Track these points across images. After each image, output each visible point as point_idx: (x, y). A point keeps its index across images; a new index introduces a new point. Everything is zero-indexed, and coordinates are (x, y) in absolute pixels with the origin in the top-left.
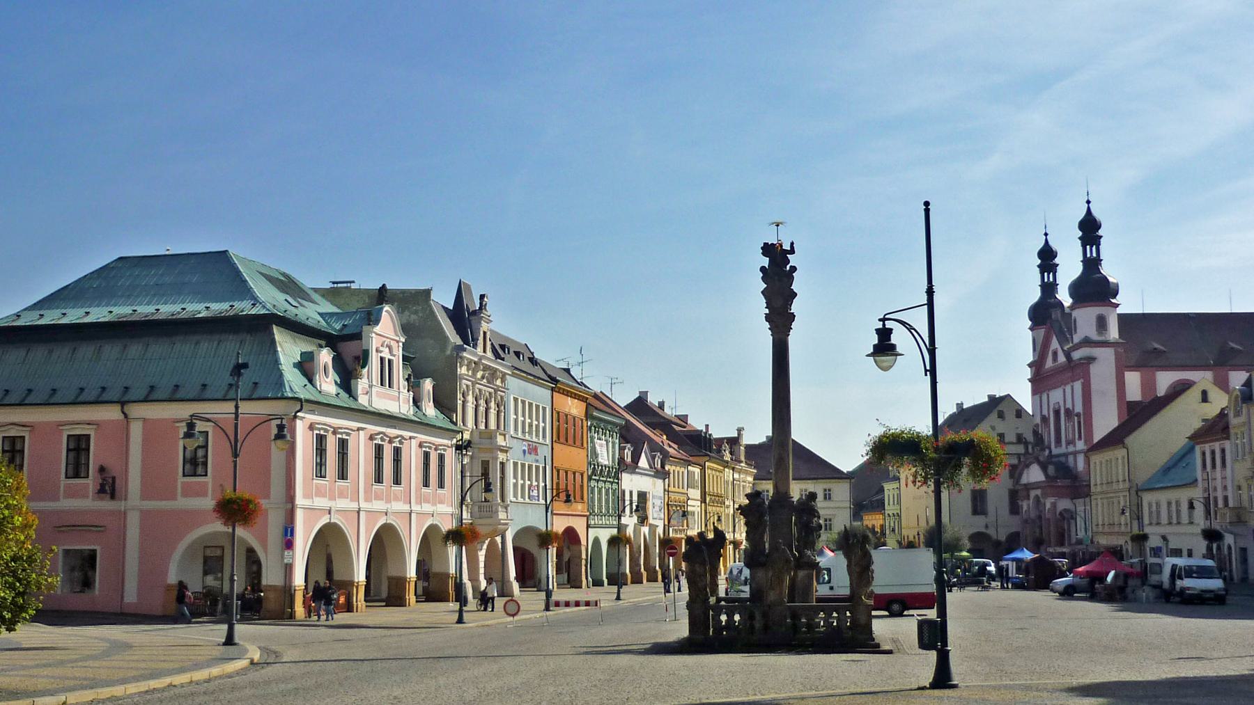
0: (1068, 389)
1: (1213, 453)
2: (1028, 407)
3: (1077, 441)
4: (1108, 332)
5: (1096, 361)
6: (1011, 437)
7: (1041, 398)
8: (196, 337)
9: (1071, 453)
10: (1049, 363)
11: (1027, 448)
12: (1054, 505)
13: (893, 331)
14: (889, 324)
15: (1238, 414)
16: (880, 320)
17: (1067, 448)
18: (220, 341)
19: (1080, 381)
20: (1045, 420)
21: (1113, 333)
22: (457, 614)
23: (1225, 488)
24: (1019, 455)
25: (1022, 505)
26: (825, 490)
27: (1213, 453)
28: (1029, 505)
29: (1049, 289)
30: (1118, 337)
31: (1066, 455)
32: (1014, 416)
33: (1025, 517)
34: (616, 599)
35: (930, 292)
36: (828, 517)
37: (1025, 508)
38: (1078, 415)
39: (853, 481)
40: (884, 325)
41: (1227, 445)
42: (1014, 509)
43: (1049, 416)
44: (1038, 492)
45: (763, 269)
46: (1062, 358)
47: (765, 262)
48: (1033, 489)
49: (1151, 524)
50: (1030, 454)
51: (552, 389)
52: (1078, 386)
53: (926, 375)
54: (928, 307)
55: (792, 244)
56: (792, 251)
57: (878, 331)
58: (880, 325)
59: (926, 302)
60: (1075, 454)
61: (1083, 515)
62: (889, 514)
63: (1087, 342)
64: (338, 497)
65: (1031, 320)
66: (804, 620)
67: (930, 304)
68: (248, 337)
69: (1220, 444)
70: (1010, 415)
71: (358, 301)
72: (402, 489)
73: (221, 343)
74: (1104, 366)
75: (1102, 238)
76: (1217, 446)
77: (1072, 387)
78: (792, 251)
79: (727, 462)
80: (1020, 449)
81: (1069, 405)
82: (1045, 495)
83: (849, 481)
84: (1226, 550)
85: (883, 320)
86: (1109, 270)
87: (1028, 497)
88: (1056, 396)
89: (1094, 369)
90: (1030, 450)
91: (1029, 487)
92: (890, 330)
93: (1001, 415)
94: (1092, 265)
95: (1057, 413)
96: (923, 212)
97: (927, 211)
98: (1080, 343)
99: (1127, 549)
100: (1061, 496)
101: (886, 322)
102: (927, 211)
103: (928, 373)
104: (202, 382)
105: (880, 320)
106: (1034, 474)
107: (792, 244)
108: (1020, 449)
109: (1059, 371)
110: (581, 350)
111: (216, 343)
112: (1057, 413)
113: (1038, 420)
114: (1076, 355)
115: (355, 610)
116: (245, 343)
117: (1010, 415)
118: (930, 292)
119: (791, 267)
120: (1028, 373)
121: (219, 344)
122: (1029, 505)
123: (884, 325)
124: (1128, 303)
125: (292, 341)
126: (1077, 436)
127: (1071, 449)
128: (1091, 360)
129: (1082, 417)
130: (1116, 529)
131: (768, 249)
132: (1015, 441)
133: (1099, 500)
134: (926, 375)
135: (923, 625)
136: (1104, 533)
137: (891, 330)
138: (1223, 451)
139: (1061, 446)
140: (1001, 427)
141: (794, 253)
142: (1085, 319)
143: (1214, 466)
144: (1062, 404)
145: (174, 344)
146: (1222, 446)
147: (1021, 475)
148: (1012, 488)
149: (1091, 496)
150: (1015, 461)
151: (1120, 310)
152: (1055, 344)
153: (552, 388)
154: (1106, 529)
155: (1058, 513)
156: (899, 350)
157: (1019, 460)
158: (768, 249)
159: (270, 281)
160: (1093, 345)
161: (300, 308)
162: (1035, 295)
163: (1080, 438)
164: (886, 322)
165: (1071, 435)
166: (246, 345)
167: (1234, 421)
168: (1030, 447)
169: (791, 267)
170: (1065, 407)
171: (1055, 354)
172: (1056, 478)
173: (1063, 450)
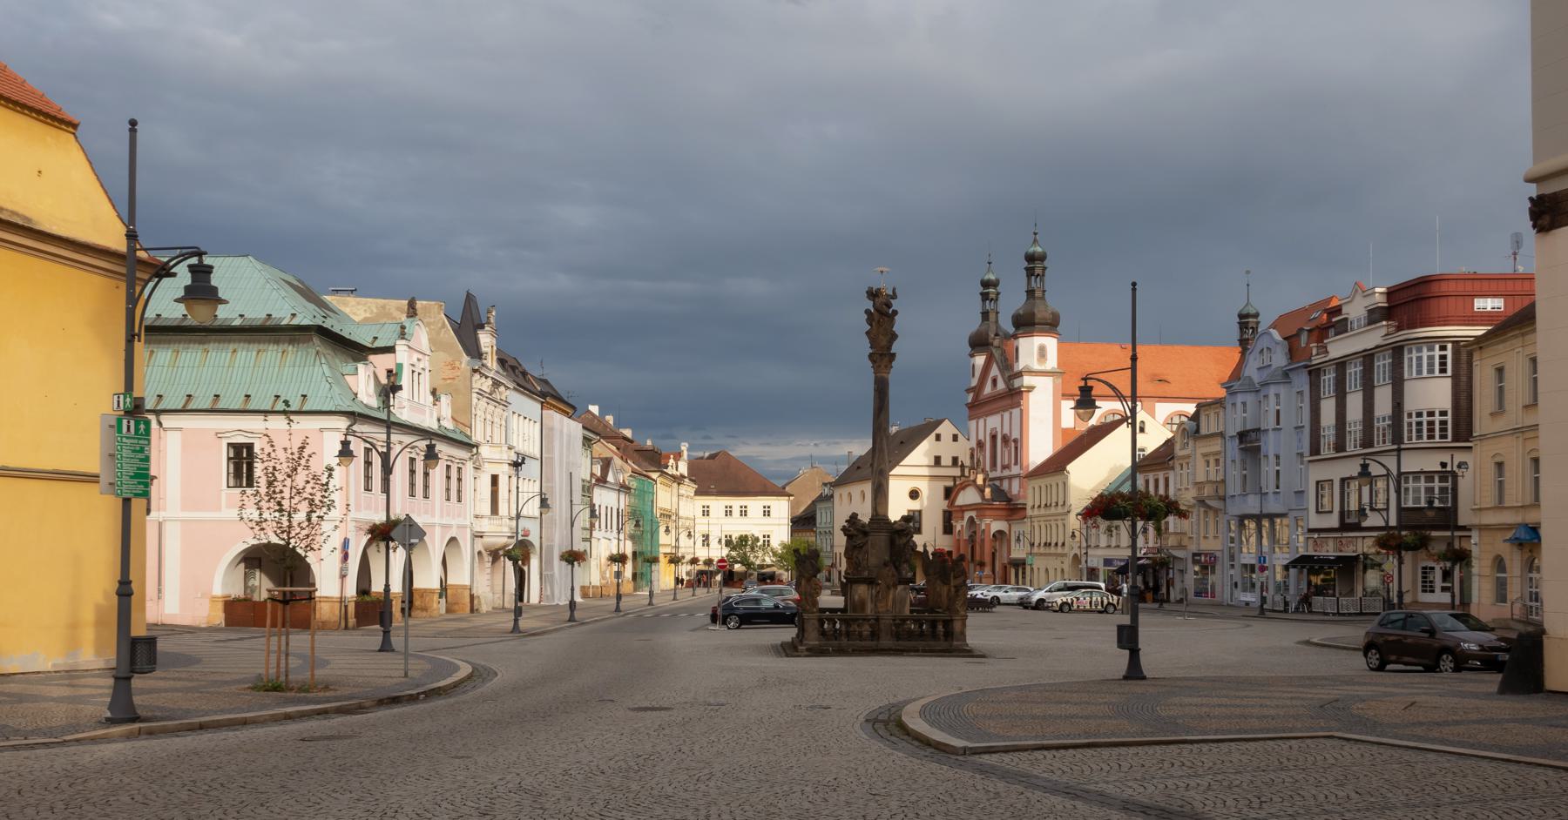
0: (1006, 415)
1: (1157, 481)
3: (1013, 466)
9: (1005, 478)
10: (988, 389)
13: (214, 270)
14: (1090, 383)
15: (1183, 448)
16: (1083, 379)
17: (1002, 472)
22: (513, 623)
24: (954, 478)
27: (1157, 481)
28: (962, 526)
30: (1056, 366)
31: (1001, 479)
33: (957, 538)
35: (1134, 359)
36: (766, 534)
39: (792, 498)
40: (1086, 383)
41: (1171, 475)
42: (948, 529)
44: (973, 514)
47: (869, 305)
48: (967, 510)
50: (966, 477)
51: (542, 403)
55: (894, 290)
56: (894, 296)
58: (1082, 384)
60: (1010, 478)
66: (913, 626)
67: (1134, 369)
68: (290, 348)
71: (365, 311)
72: (372, 496)
73: (260, 353)
76: (1161, 476)
78: (894, 296)
80: (956, 472)
81: (1006, 431)
82: (981, 517)
83: (787, 498)
85: (1085, 379)
87: (962, 518)
90: (967, 474)
91: (963, 509)
95: (994, 437)
97: (1134, 290)
101: (1088, 381)
102: (1134, 290)
105: (1083, 379)
107: (894, 290)
108: (956, 472)
109: (996, 398)
110: (542, 362)
111: (254, 353)
112: (994, 437)
115: (268, 622)
116: (288, 353)
118: (1134, 359)
119: (893, 311)
121: (258, 353)
122: (962, 526)
123: (1086, 383)
125: (332, 353)
126: (1013, 462)
127: (1006, 473)
130: (1053, 550)
131: (873, 294)
132: (950, 464)
137: (211, 267)
138: (1167, 480)
139: (996, 470)
141: (896, 298)
144: (999, 430)
146: (1166, 476)
150: (950, 484)
152: (994, 371)
154: (1042, 550)
160: (1034, 374)
164: (1088, 381)
165: (1006, 460)
167: (1179, 452)
168: (967, 471)
169: (893, 311)
170: (1002, 431)
171: (995, 381)
172: (993, 500)
173: (998, 473)
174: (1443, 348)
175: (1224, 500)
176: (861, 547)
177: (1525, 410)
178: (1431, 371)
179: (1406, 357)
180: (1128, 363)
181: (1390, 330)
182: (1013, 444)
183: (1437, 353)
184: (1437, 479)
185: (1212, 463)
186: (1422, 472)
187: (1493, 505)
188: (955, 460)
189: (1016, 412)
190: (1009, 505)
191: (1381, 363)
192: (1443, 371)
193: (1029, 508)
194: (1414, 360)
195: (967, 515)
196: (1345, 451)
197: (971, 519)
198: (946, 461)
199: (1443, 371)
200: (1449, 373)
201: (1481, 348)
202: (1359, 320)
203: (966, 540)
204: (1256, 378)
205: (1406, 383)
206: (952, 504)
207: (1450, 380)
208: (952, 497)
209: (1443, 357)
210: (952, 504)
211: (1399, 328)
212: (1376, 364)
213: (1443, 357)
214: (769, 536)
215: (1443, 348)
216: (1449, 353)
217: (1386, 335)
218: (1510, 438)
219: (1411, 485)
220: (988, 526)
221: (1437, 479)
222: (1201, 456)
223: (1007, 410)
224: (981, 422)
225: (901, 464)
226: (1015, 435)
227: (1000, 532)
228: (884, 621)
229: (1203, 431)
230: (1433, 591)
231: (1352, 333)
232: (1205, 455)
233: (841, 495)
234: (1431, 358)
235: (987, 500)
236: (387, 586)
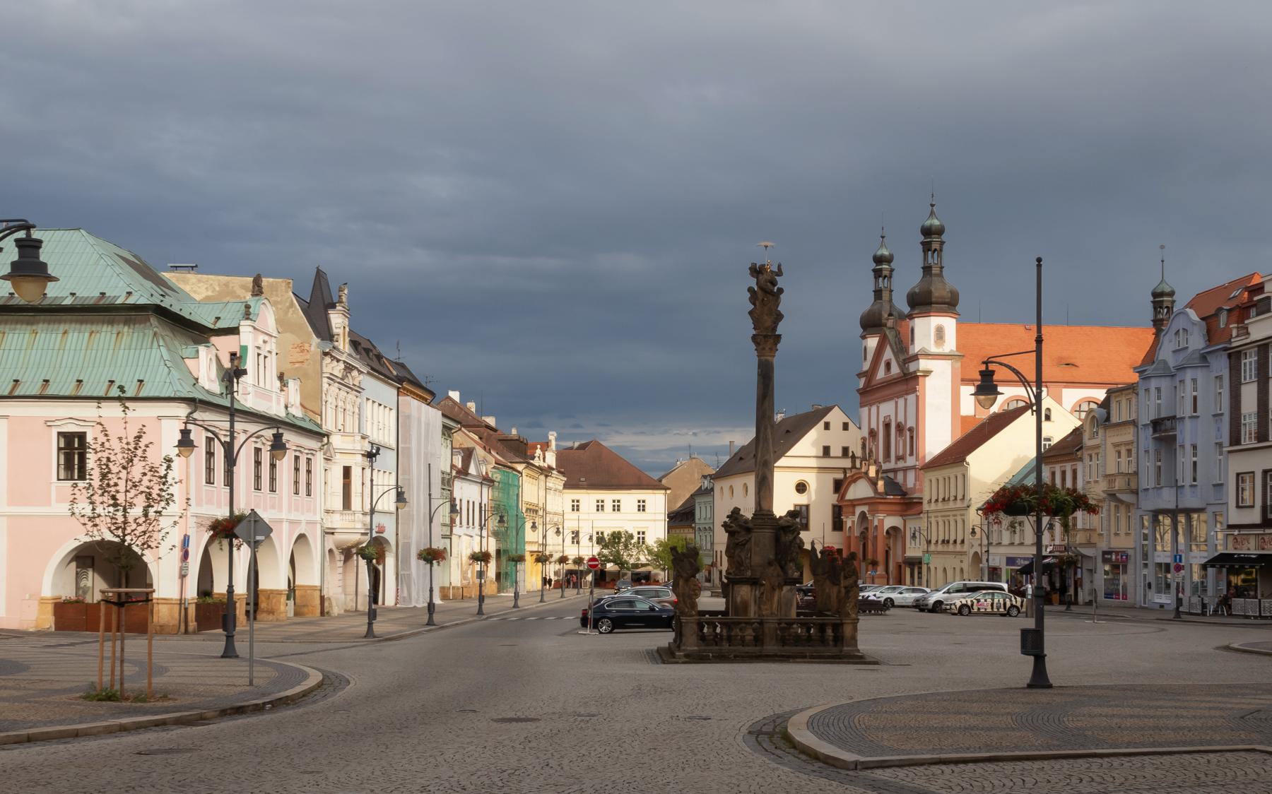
0: (901, 402)
1: (1064, 473)
5: (932, 374)
6: (836, 451)
7: (870, 410)
8: (62, 327)
10: (881, 374)
11: (854, 462)
13: (43, 245)
14: (991, 367)
16: (984, 363)
17: (896, 463)
18: (91, 333)
20: (873, 433)
24: (845, 470)
25: (846, 522)
26: (614, 501)
27: (1064, 473)
31: (895, 471)
34: (478, 614)
35: (1039, 341)
36: (641, 530)
37: (849, 524)
39: (668, 492)
40: (987, 367)
42: (838, 525)
44: (865, 509)
45: (750, 290)
46: (895, 370)
47: (753, 282)
53: (1033, 415)
54: (1037, 354)
57: (981, 373)
58: (983, 368)
59: (1035, 349)
60: (905, 470)
61: (925, 534)
62: (699, 528)
66: (799, 631)
68: (126, 329)
69: (1071, 465)
75: (945, 244)
76: (1068, 467)
78: (780, 273)
79: (1084, 504)
80: (847, 463)
81: (901, 419)
85: (986, 363)
87: (853, 513)
90: (858, 465)
91: (854, 503)
92: (993, 372)
95: (887, 426)
96: (1036, 268)
100: (890, 514)
103: (1035, 413)
104: (43, 378)
105: (984, 363)
108: (847, 463)
109: (889, 384)
111: (87, 335)
112: (887, 426)
118: (1039, 341)
122: (853, 522)
123: (987, 367)
126: (908, 452)
127: (901, 464)
131: (756, 271)
132: (841, 455)
134: (1033, 415)
135: (1025, 633)
136: (939, 553)
138: (1075, 472)
139: (890, 462)
144: (893, 418)
145: (37, 333)
150: (840, 476)
152: (888, 354)
153: (398, 388)
154: (940, 548)
155: (885, 531)
156: (51, 271)
157: (845, 475)
158: (756, 271)
159: (130, 265)
161: (167, 297)
166: (125, 338)
167: (1088, 442)
169: (778, 288)
171: (888, 365)
173: (892, 465)
175: (1137, 494)
180: (1033, 346)
182: (908, 433)
189: (911, 398)
195: (858, 510)
197: (863, 515)
204: (1172, 362)
210: (842, 498)
214: (643, 533)
220: (882, 521)
222: (1111, 446)
224: (874, 409)
225: (787, 454)
226: (911, 423)
227: (895, 529)
229: (1114, 419)
232: (1115, 445)
235: (880, 494)
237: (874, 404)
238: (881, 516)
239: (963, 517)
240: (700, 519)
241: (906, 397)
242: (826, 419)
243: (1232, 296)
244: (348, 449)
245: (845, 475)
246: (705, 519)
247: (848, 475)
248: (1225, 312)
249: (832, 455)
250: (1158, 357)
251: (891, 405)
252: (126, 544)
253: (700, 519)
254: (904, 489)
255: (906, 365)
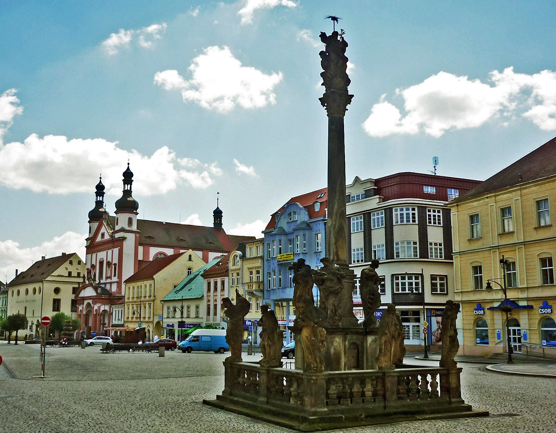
0: (110, 252)
1: (216, 283)
2: (84, 260)
4: (536, 106)
6: (74, 274)
9: (108, 283)
10: (99, 239)
12: (99, 308)
17: (106, 280)
19: (118, 248)
20: (93, 267)
21: (134, 227)
23: (216, 300)
24: (79, 283)
27: (216, 283)
29: (99, 204)
31: (105, 284)
32: (77, 264)
33: (79, 313)
38: (115, 264)
41: (226, 279)
43: (96, 264)
44: (90, 301)
47: (322, 47)
49: (168, 317)
52: (116, 250)
60: (111, 283)
63: (123, 230)
64: (174, 328)
65: (390, 103)
70: (75, 262)
74: (130, 240)
76: (219, 280)
77: (113, 251)
81: (109, 259)
82: (95, 303)
84: (276, 336)
86: (135, 196)
87: (83, 304)
88: (102, 255)
89: (125, 243)
91: (84, 299)
93: (71, 263)
94: (127, 193)
95: (101, 263)
98: (119, 230)
99: (149, 330)
106: (89, 292)
112: (101, 263)
113: (89, 266)
114: (117, 236)
117: (75, 262)
120: (85, 243)
122: (83, 308)
124: (143, 214)
127: (109, 281)
128: (124, 238)
129: (117, 265)
132: (76, 276)
133: (130, 305)
138: (223, 283)
140: (71, 268)
142: (123, 220)
143: (216, 289)
147: (79, 293)
148: (74, 298)
149: (125, 303)
151: (139, 217)
157: (79, 286)
162: (93, 206)
163: (115, 276)
171: (103, 235)
174: (413, 209)
175: (263, 292)
176: (338, 293)
177: (499, 238)
178: (408, 221)
179: (394, 213)
181: (381, 200)
182: (113, 266)
183: (411, 212)
184: (414, 278)
185: (254, 272)
186: (406, 274)
187: (540, 285)
188: (79, 274)
190: (110, 297)
191: (355, 221)
192: (414, 221)
193: (126, 298)
194: (399, 215)
195: (86, 302)
196: (394, 259)
197: (89, 304)
198: (74, 274)
199: (414, 221)
200: (417, 222)
201: (457, 205)
202: (362, 195)
203: (84, 315)
204: (286, 228)
205: (394, 226)
206: (77, 296)
207: (417, 226)
208: (77, 293)
209: (414, 214)
210: (77, 296)
211: (384, 200)
212: (372, 218)
213: (414, 214)
215: (413, 209)
216: (416, 212)
217: (379, 203)
218: (487, 252)
219: (400, 281)
220: (99, 308)
221: (414, 278)
222: (247, 269)
223: (110, 249)
224: (94, 255)
227: (105, 311)
228: (390, 379)
229: (248, 256)
230: (409, 339)
231: (352, 203)
232: (249, 269)
233: (13, 291)
234: (402, 215)
235: (100, 294)
236: (446, 370)
237: (94, 252)
238: (99, 305)
239: (128, 306)
240: (129, 298)
241: (113, 249)
242: (70, 259)
243: (318, 197)
244: (157, 413)
245: (79, 286)
246: (133, 298)
247: (80, 286)
248: (319, 204)
249: (72, 276)
250: (277, 226)
251: (105, 252)
252: (234, 303)
253: (129, 298)
254: (110, 292)
255: (113, 235)
